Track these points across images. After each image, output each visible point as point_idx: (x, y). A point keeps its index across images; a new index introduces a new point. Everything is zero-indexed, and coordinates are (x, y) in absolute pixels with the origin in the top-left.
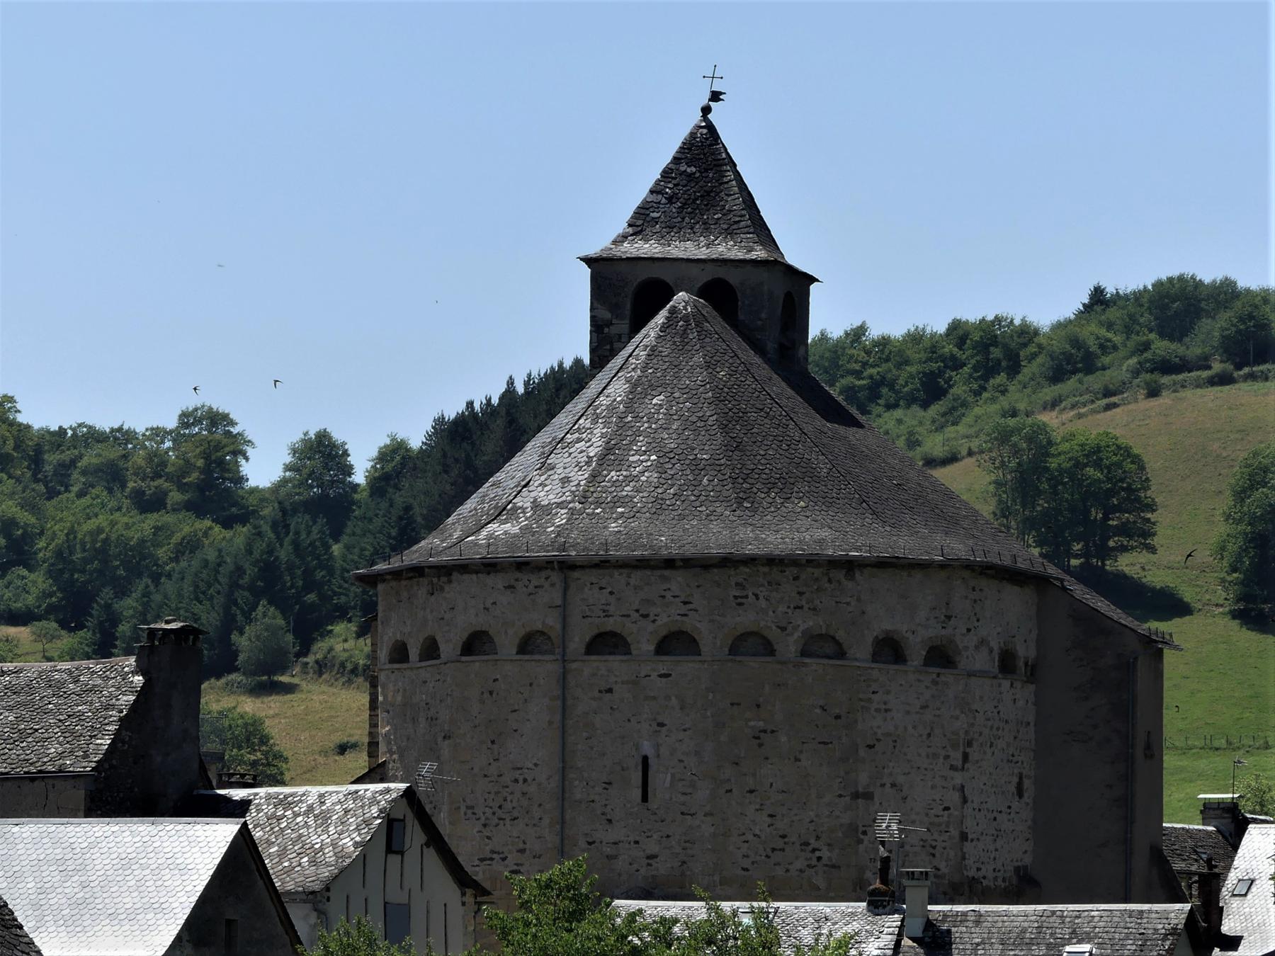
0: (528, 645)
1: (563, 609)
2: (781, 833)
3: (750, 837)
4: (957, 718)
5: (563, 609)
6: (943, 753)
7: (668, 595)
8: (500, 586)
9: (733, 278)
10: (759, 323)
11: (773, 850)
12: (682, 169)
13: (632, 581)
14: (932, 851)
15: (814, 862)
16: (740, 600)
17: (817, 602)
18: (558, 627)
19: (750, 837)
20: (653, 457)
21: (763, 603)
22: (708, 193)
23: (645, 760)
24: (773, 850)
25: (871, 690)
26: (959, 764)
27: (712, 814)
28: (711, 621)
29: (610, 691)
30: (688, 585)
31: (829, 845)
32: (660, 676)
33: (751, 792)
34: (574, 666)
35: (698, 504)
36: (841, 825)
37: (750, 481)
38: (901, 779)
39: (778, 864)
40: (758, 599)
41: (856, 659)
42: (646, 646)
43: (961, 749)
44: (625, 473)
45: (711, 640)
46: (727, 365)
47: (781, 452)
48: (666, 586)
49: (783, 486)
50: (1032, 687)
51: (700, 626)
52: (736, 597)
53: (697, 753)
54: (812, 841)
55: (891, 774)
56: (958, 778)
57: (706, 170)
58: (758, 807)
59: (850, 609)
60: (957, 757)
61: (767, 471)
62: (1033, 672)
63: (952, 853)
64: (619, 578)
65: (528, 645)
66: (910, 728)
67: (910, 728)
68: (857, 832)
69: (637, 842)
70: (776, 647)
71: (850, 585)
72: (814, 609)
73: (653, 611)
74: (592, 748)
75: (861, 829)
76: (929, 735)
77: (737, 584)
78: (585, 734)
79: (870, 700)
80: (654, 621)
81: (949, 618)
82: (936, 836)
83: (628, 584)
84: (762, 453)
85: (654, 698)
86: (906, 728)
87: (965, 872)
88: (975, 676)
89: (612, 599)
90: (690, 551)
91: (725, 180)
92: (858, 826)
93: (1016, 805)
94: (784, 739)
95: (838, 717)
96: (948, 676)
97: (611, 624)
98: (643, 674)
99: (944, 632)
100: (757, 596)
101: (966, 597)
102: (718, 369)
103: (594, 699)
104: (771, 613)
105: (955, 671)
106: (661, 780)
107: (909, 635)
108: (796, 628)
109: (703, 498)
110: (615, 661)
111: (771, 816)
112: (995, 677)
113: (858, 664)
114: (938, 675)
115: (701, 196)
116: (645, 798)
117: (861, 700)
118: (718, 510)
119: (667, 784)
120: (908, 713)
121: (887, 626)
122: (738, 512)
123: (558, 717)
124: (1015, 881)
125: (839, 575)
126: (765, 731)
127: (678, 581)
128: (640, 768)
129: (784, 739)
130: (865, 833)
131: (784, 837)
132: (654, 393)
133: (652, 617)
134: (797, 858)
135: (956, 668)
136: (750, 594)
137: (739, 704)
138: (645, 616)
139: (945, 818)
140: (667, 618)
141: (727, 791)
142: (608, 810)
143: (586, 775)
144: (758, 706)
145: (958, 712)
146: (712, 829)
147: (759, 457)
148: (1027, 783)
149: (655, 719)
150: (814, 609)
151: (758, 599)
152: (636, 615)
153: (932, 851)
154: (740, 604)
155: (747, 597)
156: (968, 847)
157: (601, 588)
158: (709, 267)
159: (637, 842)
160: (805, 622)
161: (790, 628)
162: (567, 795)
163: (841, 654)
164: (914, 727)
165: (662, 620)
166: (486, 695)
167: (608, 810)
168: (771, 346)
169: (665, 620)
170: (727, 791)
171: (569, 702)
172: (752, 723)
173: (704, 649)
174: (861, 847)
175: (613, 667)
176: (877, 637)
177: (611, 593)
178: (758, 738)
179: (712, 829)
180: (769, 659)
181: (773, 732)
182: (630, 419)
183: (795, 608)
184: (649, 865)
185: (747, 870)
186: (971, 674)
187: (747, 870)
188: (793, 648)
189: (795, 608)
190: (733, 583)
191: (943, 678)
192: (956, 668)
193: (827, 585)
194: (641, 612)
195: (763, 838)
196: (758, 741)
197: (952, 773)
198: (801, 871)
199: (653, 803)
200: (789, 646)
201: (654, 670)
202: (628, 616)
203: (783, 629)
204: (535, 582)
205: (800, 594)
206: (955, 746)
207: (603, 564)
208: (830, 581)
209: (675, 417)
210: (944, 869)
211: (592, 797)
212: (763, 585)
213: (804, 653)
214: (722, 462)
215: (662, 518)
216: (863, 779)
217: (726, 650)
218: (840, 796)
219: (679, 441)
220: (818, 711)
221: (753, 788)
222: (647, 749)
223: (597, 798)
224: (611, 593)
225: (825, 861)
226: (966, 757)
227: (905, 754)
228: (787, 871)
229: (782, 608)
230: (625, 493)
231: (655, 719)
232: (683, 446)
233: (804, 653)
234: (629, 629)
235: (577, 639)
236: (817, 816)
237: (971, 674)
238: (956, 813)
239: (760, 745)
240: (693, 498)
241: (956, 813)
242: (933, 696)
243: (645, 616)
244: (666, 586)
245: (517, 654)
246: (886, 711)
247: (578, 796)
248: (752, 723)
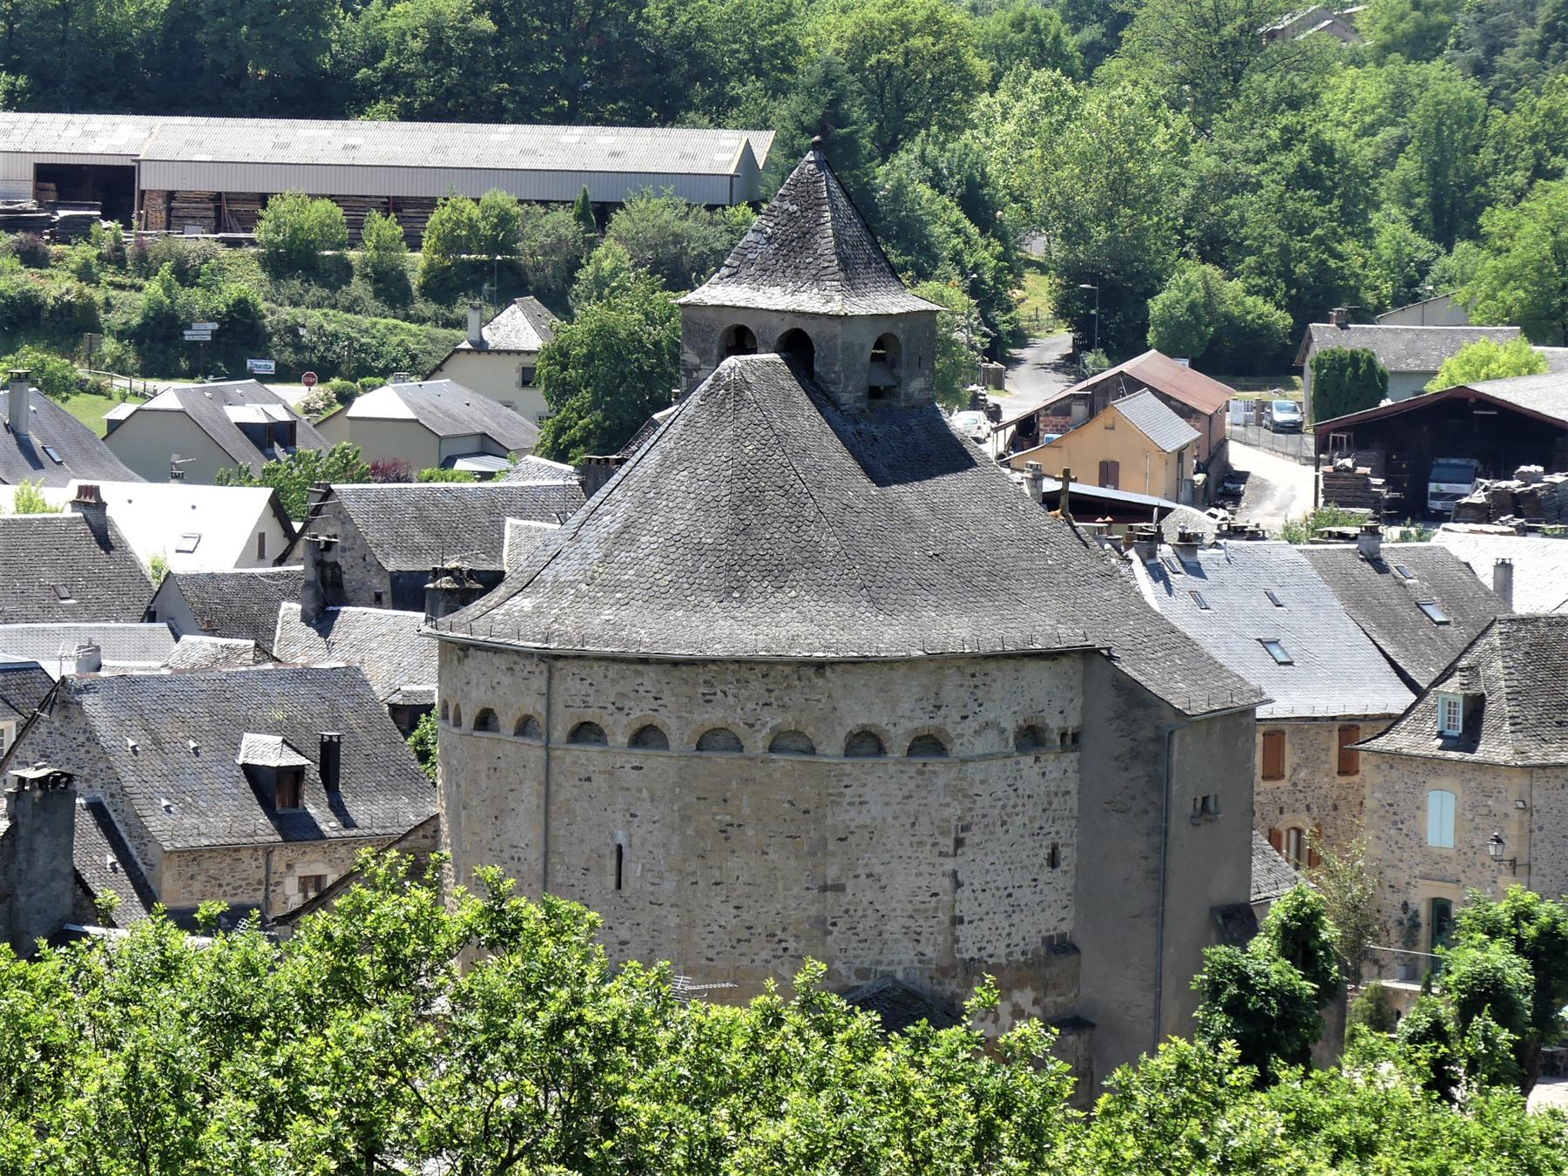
0: (524, 727)
1: (548, 696)
2: (747, 924)
3: (715, 928)
4: (948, 805)
5: (548, 696)
6: (931, 840)
7: (641, 689)
8: (503, 667)
9: (811, 330)
10: (833, 375)
11: (739, 941)
12: (785, 207)
13: (610, 675)
14: (916, 937)
15: (780, 953)
16: (708, 697)
17: (786, 699)
18: (544, 713)
19: (715, 928)
20: (661, 540)
21: (731, 700)
22: (805, 234)
23: (620, 847)
24: (739, 941)
25: (843, 784)
26: (951, 850)
27: (677, 906)
28: (680, 718)
29: (589, 779)
30: (658, 681)
31: (796, 936)
32: (634, 768)
33: (717, 884)
34: (557, 753)
35: (689, 592)
36: (809, 917)
37: (746, 568)
38: (878, 869)
39: (744, 955)
40: (726, 696)
41: (825, 756)
42: (620, 737)
43: (953, 835)
44: (633, 555)
45: (680, 735)
46: (758, 438)
47: (789, 535)
48: (640, 681)
49: (778, 573)
50: (1073, 756)
51: (668, 721)
52: (704, 694)
53: (664, 845)
54: (779, 932)
55: (866, 865)
56: (949, 864)
57: (806, 210)
58: (724, 899)
59: (820, 706)
60: (948, 843)
61: (767, 557)
62: (1072, 740)
63: (940, 939)
64: (598, 670)
65: (524, 727)
66: (890, 819)
67: (890, 819)
68: (824, 925)
69: (611, 928)
70: (744, 743)
71: (821, 682)
72: (783, 706)
73: (628, 704)
74: (572, 834)
75: (830, 920)
76: (913, 824)
77: (705, 682)
78: (566, 820)
79: (841, 795)
80: (628, 714)
81: (938, 707)
82: (921, 922)
83: (606, 677)
84: (768, 536)
85: (628, 789)
86: (884, 819)
87: (958, 956)
88: (973, 761)
89: (591, 691)
90: (660, 650)
91: (822, 221)
92: (826, 919)
93: (1046, 875)
94: (751, 833)
95: (806, 812)
96: (935, 764)
97: (590, 715)
98: (618, 765)
99: (932, 722)
100: (725, 693)
101: (961, 686)
102: (747, 443)
103: (575, 786)
104: (739, 710)
105: (945, 760)
106: (632, 870)
107: (890, 727)
108: (764, 725)
109: (696, 586)
110: (593, 750)
111: (737, 908)
112: (1009, 756)
113: (826, 760)
114: (925, 765)
115: (799, 238)
116: (619, 886)
117: (830, 795)
118: (706, 600)
119: (638, 874)
120: (887, 804)
121: (863, 720)
122: (725, 603)
123: (542, 803)
124: (1043, 951)
125: (810, 672)
126: (732, 825)
127: (651, 673)
128: (615, 856)
129: (751, 833)
130: (834, 924)
131: (750, 928)
132: (680, 468)
133: (626, 711)
134: (763, 949)
135: (947, 756)
136: (719, 692)
137: (705, 799)
138: (620, 709)
139: (933, 904)
140: (639, 713)
141: (693, 883)
142: (586, 895)
143: (566, 860)
144: (725, 801)
145: (949, 800)
146: (677, 920)
147: (763, 541)
148: (1064, 852)
149: (628, 810)
150: (783, 706)
151: (726, 696)
152: (613, 707)
153: (916, 937)
154: (708, 701)
155: (715, 694)
156: (961, 930)
157: (582, 679)
158: (788, 317)
159: (611, 928)
160: (774, 719)
161: (757, 727)
162: (550, 878)
163: (811, 751)
164: (895, 818)
165: (636, 713)
166: (492, 771)
167: (586, 895)
168: (849, 395)
169: (639, 714)
170: (693, 883)
171: (553, 788)
172: (718, 817)
173: (673, 744)
174: (830, 939)
175: (587, 754)
176: (851, 732)
177: (591, 684)
178: (725, 831)
179: (677, 920)
180: (736, 755)
181: (739, 826)
182: (652, 495)
183: (764, 705)
184: (622, 950)
185: (712, 960)
186: (964, 761)
187: (712, 960)
188: (760, 745)
189: (764, 705)
190: (701, 681)
191: (930, 767)
192: (947, 756)
193: (797, 683)
194: (617, 705)
195: (729, 928)
196: (724, 835)
197: (941, 860)
198: (767, 961)
199: (626, 890)
200: (757, 742)
201: (627, 762)
202: (605, 708)
203: (751, 726)
204: (529, 668)
205: (769, 691)
206: (945, 833)
207: (580, 657)
208: (799, 679)
209: (692, 496)
210: (930, 952)
211: (572, 882)
212: (731, 683)
213: (772, 749)
214: (724, 547)
215: (652, 606)
216: (832, 872)
217: (694, 746)
218: (808, 889)
219: (689, 523)
220: (786, 805)
221: (719, 880)
222: (621, 838)
223: (576, 883)
224: (591, 684)
225: (791, 951)
226: (959, 843)
227: (884, 844)
228: (753, 961)
229: (750, 706)
230: (627, 577)
231: (628, 810)
232: (691, 528)
233: (772, 749)
234: (606, 720)
235: (559, 728)
236: (784, 908)
237: (964, 761)
238: (946, 898)
239: (727, 839)
240: (686, 586)
241: (946, 898)
242: (918, 786)
243: (620, 709)
244: (640, 681)
245: (515, 734)
246: (861, 803)
247: (560, 880)
248: (718, 817)
